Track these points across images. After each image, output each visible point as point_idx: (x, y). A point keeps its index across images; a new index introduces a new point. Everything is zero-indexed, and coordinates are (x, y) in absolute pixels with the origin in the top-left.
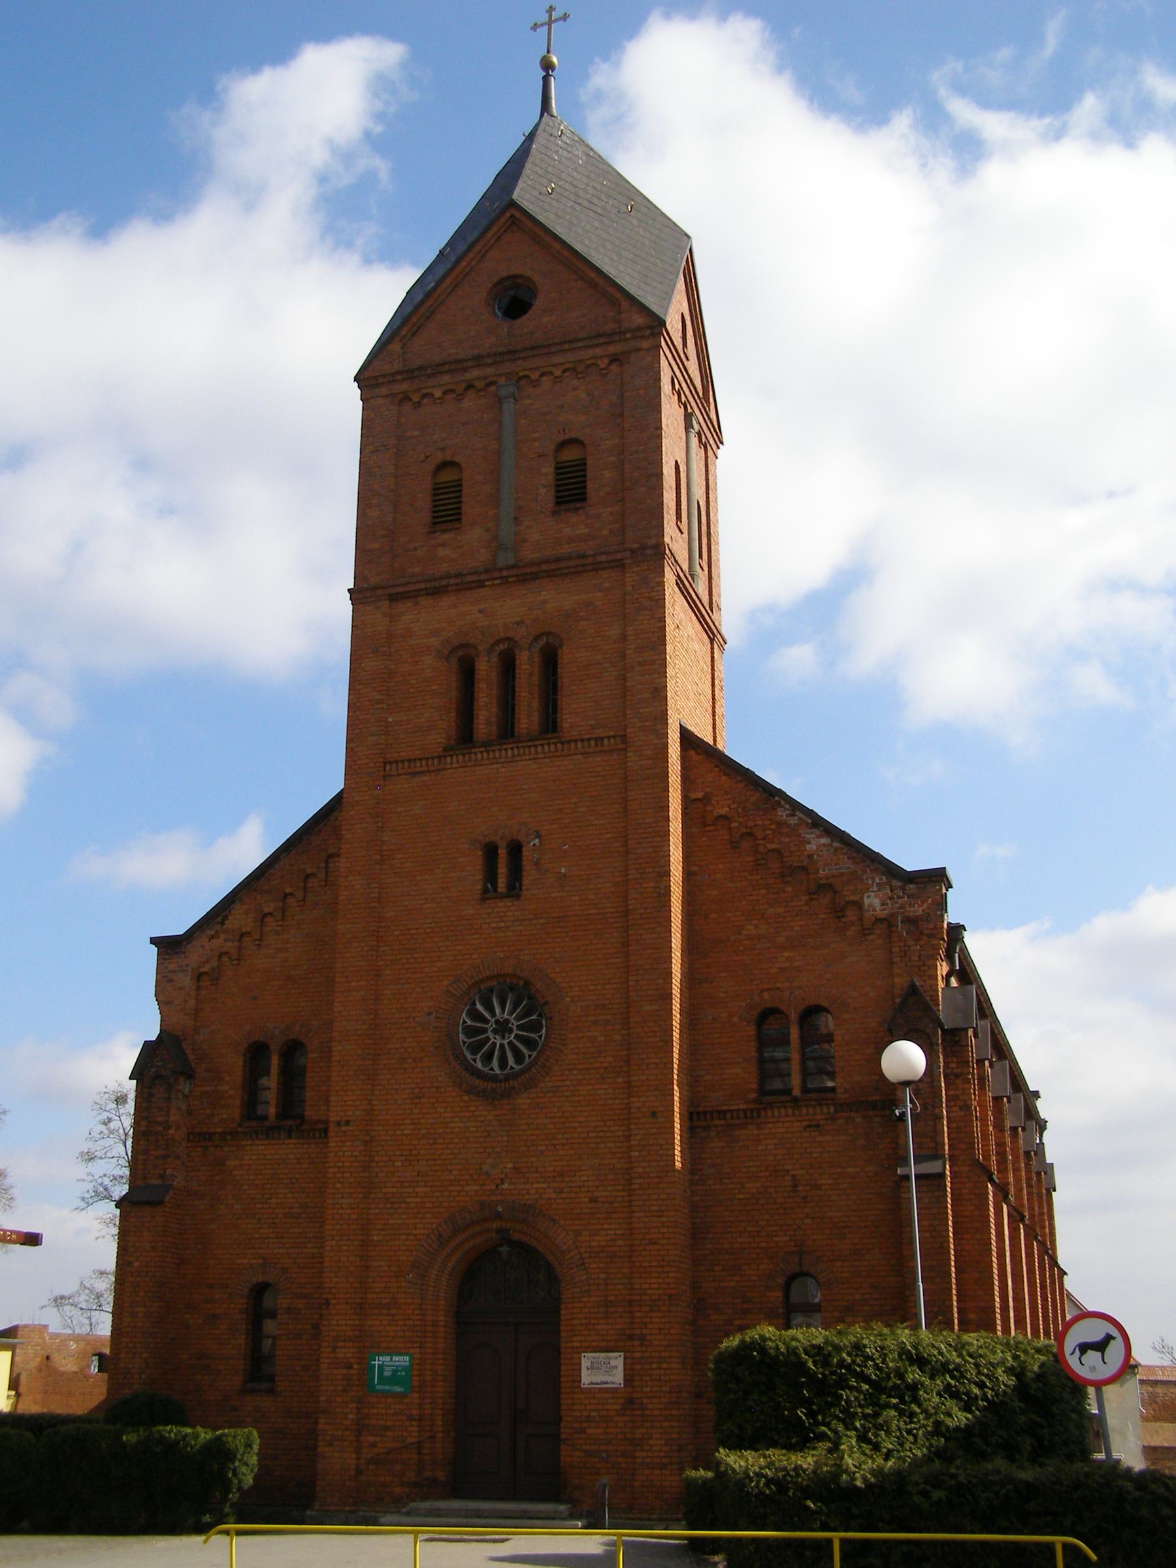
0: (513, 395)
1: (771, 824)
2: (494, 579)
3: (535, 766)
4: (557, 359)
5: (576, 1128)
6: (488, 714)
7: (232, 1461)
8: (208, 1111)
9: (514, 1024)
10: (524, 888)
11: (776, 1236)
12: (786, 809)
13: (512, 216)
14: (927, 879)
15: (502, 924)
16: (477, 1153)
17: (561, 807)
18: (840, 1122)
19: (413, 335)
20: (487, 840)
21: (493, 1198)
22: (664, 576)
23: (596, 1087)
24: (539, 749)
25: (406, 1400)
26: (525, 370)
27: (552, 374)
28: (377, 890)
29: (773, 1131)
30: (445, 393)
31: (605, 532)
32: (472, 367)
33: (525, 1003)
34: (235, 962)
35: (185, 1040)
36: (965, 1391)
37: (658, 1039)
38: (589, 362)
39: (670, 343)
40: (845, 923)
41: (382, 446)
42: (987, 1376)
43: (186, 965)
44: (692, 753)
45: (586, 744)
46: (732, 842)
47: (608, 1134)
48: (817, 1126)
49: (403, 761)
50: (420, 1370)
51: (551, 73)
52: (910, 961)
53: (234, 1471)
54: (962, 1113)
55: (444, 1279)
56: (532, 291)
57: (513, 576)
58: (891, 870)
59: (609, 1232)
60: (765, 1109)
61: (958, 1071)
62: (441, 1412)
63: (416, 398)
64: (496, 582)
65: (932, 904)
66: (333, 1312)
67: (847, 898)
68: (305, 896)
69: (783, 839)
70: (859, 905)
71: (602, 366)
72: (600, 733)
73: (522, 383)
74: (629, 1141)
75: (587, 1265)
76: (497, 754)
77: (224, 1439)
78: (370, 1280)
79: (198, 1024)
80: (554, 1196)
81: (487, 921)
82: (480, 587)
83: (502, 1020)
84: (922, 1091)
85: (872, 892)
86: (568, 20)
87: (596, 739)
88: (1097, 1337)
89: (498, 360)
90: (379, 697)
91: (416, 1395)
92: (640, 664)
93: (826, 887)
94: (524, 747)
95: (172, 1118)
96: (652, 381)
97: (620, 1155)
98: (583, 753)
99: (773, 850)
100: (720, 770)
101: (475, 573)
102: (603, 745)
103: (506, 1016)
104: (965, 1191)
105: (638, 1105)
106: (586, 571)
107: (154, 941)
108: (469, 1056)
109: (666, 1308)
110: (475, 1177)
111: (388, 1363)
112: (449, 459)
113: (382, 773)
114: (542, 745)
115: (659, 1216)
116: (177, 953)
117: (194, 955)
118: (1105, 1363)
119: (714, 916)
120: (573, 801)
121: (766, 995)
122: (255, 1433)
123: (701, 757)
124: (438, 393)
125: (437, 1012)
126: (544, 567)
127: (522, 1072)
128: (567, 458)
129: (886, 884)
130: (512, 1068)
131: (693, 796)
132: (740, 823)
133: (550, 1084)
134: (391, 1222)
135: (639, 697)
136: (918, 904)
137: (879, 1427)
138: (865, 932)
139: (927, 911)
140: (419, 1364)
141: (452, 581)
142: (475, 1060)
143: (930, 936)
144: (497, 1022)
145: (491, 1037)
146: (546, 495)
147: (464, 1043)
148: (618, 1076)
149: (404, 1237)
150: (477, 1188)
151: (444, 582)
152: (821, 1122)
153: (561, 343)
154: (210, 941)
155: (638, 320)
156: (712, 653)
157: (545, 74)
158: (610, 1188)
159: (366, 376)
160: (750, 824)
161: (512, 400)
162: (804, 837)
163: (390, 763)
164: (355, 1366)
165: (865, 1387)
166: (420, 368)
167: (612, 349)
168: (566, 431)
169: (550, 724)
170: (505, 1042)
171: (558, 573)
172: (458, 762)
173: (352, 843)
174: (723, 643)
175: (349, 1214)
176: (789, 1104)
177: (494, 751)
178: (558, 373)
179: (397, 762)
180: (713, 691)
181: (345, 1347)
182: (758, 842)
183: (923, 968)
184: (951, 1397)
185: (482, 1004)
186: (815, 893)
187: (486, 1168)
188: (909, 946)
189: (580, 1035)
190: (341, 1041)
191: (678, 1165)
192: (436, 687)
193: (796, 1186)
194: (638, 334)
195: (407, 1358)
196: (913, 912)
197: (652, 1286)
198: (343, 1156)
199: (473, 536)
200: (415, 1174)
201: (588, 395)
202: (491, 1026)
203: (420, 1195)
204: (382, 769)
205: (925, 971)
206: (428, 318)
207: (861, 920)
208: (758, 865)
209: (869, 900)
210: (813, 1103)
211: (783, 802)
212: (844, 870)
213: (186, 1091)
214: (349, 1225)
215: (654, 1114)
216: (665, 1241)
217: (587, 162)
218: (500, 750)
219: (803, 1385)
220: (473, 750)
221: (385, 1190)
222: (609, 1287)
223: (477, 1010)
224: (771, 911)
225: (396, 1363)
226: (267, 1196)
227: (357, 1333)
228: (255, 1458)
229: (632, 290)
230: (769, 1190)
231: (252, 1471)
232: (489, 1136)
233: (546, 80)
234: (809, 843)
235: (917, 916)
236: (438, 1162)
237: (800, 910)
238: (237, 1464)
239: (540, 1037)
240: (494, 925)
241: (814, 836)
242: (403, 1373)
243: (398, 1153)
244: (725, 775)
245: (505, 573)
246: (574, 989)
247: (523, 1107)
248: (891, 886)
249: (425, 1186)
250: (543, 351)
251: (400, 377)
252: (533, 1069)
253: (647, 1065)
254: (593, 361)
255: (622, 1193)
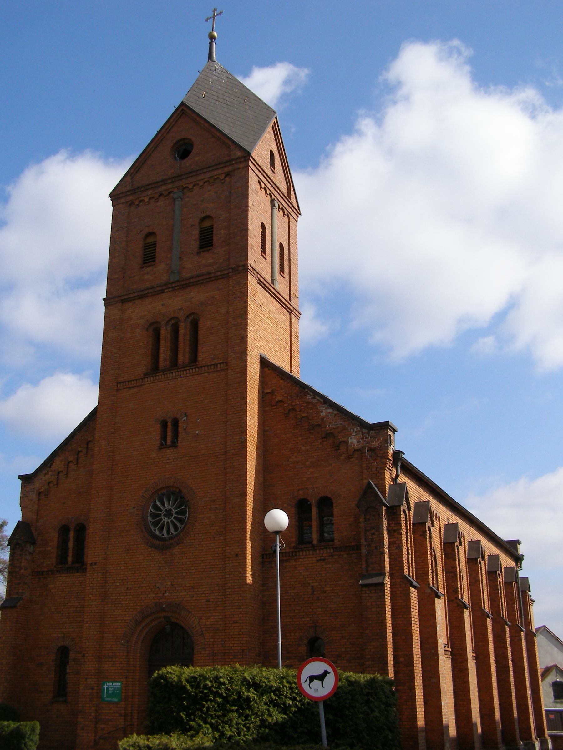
0: (180, 197)
1: (304, 403)
2: (168, 288)
3: (186, 380)
4: (200, 177)
5: (200, 563)
6: (165, 356)
7: (24, 739)
8: (42, 561)
9: (174, 512)
10: (179, 442)
11: (303, 618)
12: (311, 395)
13: (183, 110)
14: (380, 428)
15: (168, 461)
16: (154, 578)
17: (197, 400)
18: (336, 557)
19: (137, 172)
20: (163, 419)
21: (161, 601)
22: (247, 280)
23: (210, 542)
24: (188, 371)
25: (119, 706)
26: (186, 184)
27: (198, 184)
28: (111, 447)
29: (302, 563)
30: (150, 199)
31: (221, 261)
32: (162, 185)
33: (179, 500)
34: (55, 486)
35: (32, 525)
36: (282, 702)
37: (239, 516)
38: (215, 177)
39: (255, 164)
40: (339, 452)
41: (121, 228)
42: (297, 694)
43: (34, 489)
44: (266, 370)
45: (209, 367)
46: (285, 414)
47: (216, 566)
48: (324, 560)
49: (126, 382)
50: (125, 690)
51: (213, 41)
52: (372, 471)
53: (25, 744)
54: (397, 551)
55: (140, 643)
56: (192, 145)
57: (178, 286)
58: (362, 424)
59: (215, 617)
60: (299, 551)
61: (395, 528)
62: (137, 712)
63: (136, 203)
64: (170, 290)
65: (383, 440)
66: (86, 660)
67: (340, 440)
68: (87, 452)
69: (309, 411)
70: (346, 443)
71: (222, 178)
72: (216, 361)
73: (185, 190)
74: (225, 570)
75: (204, 635)
76: (168, 375)
77: (20, 727)
78: (104, 644)
79: (39, 517)
80: (189, 599)
81: (162, 459)
82: (162, 293)
83: (168, 509)
84: (375, 540)
85: (353, 436)
86: (222, 14)
87: (214, 365)
88: (320, 672)
89: (174, 180)
90: (116, 351)
91: (123, 703)
92: (235, 325)
93: (329, 435)
94: (181, 371)
95: (23, 564)
96: (244, 183)
97: (221, 577)
98: (208, 373)
99: (305, 417)
100: (279, 378)
101: (160, 286)
102: (217, 367)
103: (170, 508)
104: (398, 592)
105: (229, 551)
106: (211, 281)
107: (20, 477)
108: (152, 528)
109: (241, 656)
110: (153, 590)
111: (111, 687)
112: (151, 231)
113: (116, 388)
114: (189, 370)
115: (239, 609)
116: (30, 483)
117: (37, 484)
118: (323, 687)
119: (276, 452)
120: (202, 397)
121: (300, 492)
122: (38, 724)
123: (270, 371)
124: (146, 199)
125: (137, 507)
126: (192, 280)
127: (176, 536)
128: (205, 226)
129: (359, 431)
130: (172, 534)
131: (266, 391)
132: (289, 404)
133: (189, 541)
134: (114, 614)
135: (234, 342)
136: (375, 441)
137: (225, 723)
138: (349, 457)
139: (380, 444)
140: (125, 687)
141: (149, 291)
142: (155, 530)
143: (382, 457)
144: (166, 510)
145: (163, 518)
146: (194, 244)
147: (151, 522)
148: (221, 537)
149: (120, 621)
150: (154, 595)
151: (146, 292)
152: (326, 558)
153: (203, 169)
154: (44, 476)
155: (238, 154)
156: (290, 319)
157: (210, 41)
158: (216, 594)
159: (114, 194)
160: (294, 404)
161: (179, 199)
162: (320, 409)
163: (120, 383)
164: (95, 688)
165: (220, 700)
166: (138, 188)
167: (226, 170)
168: (205, 212)
169: (194, 358)
170: (169, 521)
171: (198, 283)
172: (150, 381)
173: (101, 424)
174: (298, 314)
175: (95, 610)
176: (310, 549)
177: (167, 374)
178: (201, 184)
179: (123, 382)
180: (291, 338)
181: (91, 678)
182: (297, 413)
183: (378, 475)
184: (274, 706)
185: (159, 501)
186: (324, 438)
187: (158, 585)
188: (371, 463)
189: (203, 516)
190: (93, 523)
191: (249, 580)
192: (141, 344)
193: (313, 592)
194: (238, 161)
195: (120, 684)
196: (374, 445)
197: (235, 645)
198: (93, 581)
199: (161, 268)
200: (126, 589)
201: (215, 193)
202: (164, 512)
203: (128, 600)
204: (116, 386)
205: (379, 476)
206: (143, 163)
207: (347, 451)
208: (297, 425)
209: (351, 440)
210: (323, 548)
211: (309, 392)
212: (339, 425)
213: (31, 551)
214: (95, 616)
215: (237, 555)
216: (241, 622)
217: (227, 81)
218: (170, 373)
219: (184, 699)
220: (157, 374)
221: (111, 598)
222: (215, 646)
223: (157, 505)
224: (303, 448)
225: (115, 687)
226: (66, 602)
227: (96, 671)
228: (38, 737)
229: (236, 140)
230: (301, 594)
231: (35, 744)
232: (160, 569)
233: (211, 44)
234: (322, 412)
235: (375, 447)
236: (136, 583)
237: (318, 447)
238: (27, 740)
239: (186, 517)
240: (164, 462)
241: (324, 408)
242: (118, 692)
243: (118, 578)
244: (282, 380)
245: (173, 285)
246: (201, 492)
247: (176, 553)
248: (362, 432)
249: (130, 595)
250: (194, 174)
251: (129, 193)
252: (181, 534)
253: (234, 530)
254: (217, 176)
255: (222, 597)
